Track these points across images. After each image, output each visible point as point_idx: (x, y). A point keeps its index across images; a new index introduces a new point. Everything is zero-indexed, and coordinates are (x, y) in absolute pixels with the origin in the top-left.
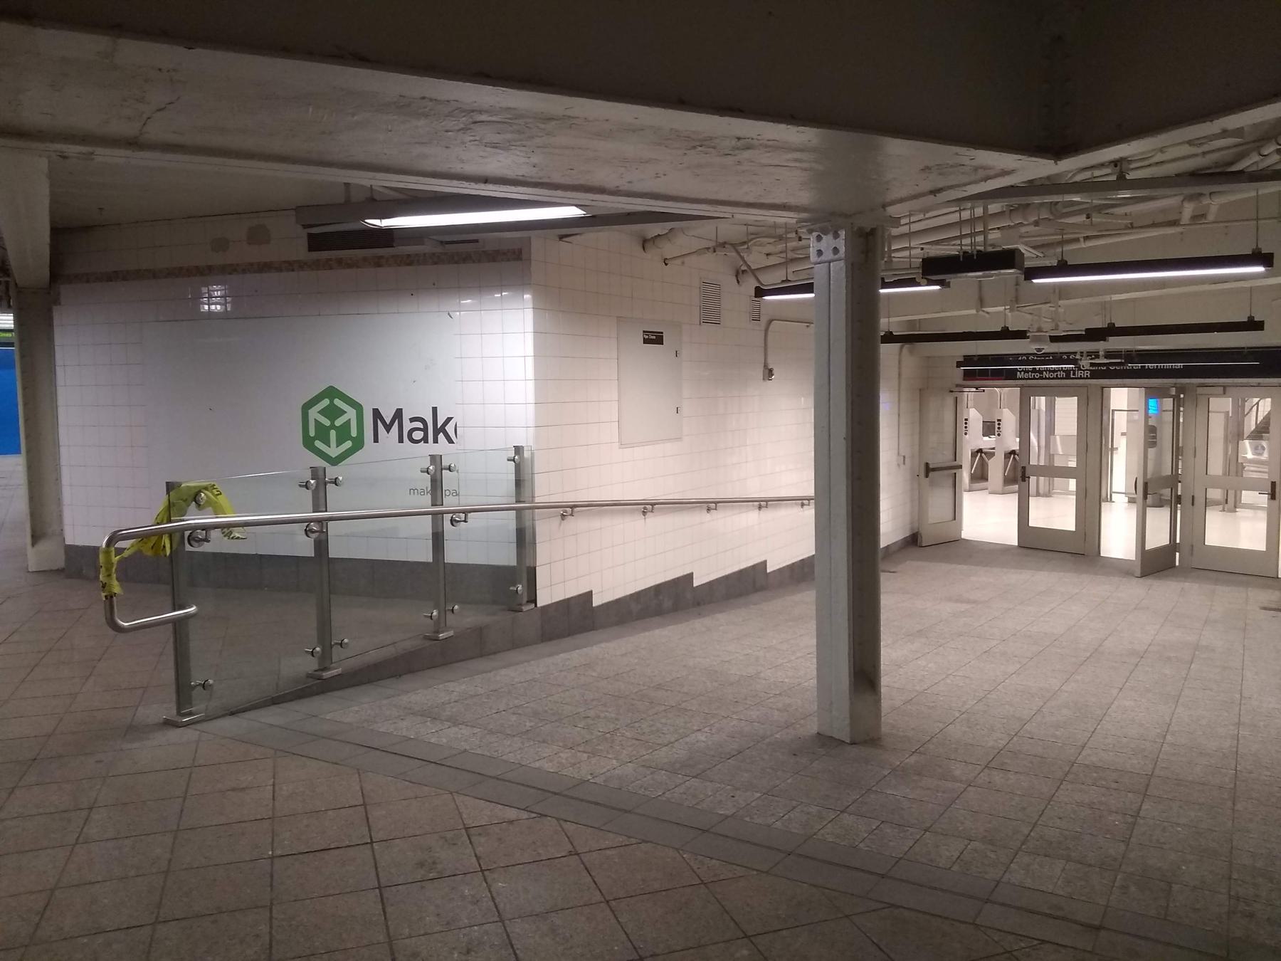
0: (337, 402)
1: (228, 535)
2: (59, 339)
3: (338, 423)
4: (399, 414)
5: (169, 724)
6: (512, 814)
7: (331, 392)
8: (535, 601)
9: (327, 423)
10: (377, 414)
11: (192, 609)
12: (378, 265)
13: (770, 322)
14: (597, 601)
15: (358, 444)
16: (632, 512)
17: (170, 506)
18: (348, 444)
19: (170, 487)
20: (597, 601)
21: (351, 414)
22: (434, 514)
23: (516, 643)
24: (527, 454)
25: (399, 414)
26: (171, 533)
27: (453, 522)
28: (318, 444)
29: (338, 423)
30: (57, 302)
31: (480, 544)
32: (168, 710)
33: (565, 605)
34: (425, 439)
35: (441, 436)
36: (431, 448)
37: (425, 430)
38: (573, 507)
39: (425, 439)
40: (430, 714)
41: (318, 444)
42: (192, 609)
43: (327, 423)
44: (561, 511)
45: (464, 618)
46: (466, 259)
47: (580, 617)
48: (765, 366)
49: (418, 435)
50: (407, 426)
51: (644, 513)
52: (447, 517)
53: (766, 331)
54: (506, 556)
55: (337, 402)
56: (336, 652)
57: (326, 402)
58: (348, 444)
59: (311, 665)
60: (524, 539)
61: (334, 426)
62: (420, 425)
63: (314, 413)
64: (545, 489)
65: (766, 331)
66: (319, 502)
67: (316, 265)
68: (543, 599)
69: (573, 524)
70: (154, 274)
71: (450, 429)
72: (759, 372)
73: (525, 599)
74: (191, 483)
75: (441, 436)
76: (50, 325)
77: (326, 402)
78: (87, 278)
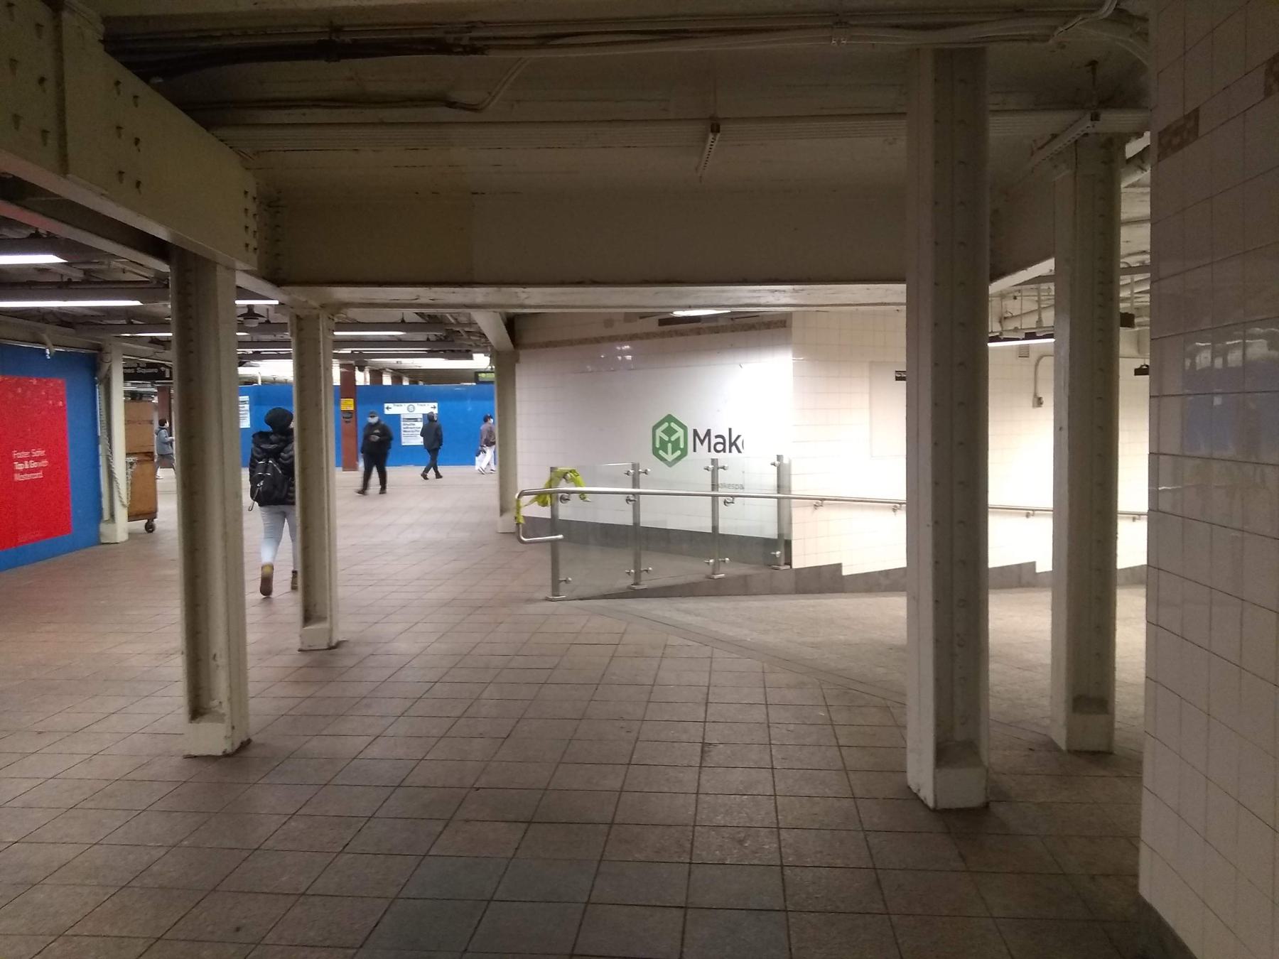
0: (673, 425)
1: (583, 499)
2: (518, 385)
3: (673, 438)
4: (708, 433)
5: (547, 599)
6: (690, 643)
7: (670, 418)
8: (789, 563)
9: (666, 438)
10: (696, 433)
11: (560, 536)
12: (699, 334)
13: (1039, 360)
14: (845, 572)
15: (684, 453)
16: (884, 508)
17: (551, 480)
18: (678, 453)
19: (552, 469)
20: (845, 572)
21: (680, 432)
22: (713, 496)
23: (774, 591)
24: (785, 461)
25: (708, 433)
26: (551, 494)
27: (725, 502)
28: (661, 452)
29: (673, 438)
30: (517, 361)
31: (750, 519)
32: (547, 592)
33: (817, 571)
34: (724, 450)
35: (734, 448)
36: (714, 455)
37: (724, 444)
38: (823, 500)
39: (724, 450)
40: (687, 612)
41: (661, 452)
42: (560, 536)
43: (666, 438)
44: (814, 502)
45: (729, 569)
46: (752, 327)
47: (828, 580)
48: (1035, 395)
49: (720, 447)
50: (714, 441)
51: (894, 510)
52: (721, 500)
53: (1037, 365)
54: (771, 532)
55: (673, 425)
56: (644, 575)
57: (666, 425)
58: (678, 453)
59: (630, 581)
60: (784, 519)
61: (671, 440)
62: (721, 440)
63: (659, 432)
64: (798, 486)
65: (1037, 365)
66: (636, 483)
67: (663, 335)
68: (797, 564)
69: (822, 512)
70: (571, 343)
71: (739, 443)
72: (1029, 400)
73: (783, 562)
74: (562, 468)
75: (734, 448)
76: (514, 374)
77: (666, 425)
78: (534, 346)
